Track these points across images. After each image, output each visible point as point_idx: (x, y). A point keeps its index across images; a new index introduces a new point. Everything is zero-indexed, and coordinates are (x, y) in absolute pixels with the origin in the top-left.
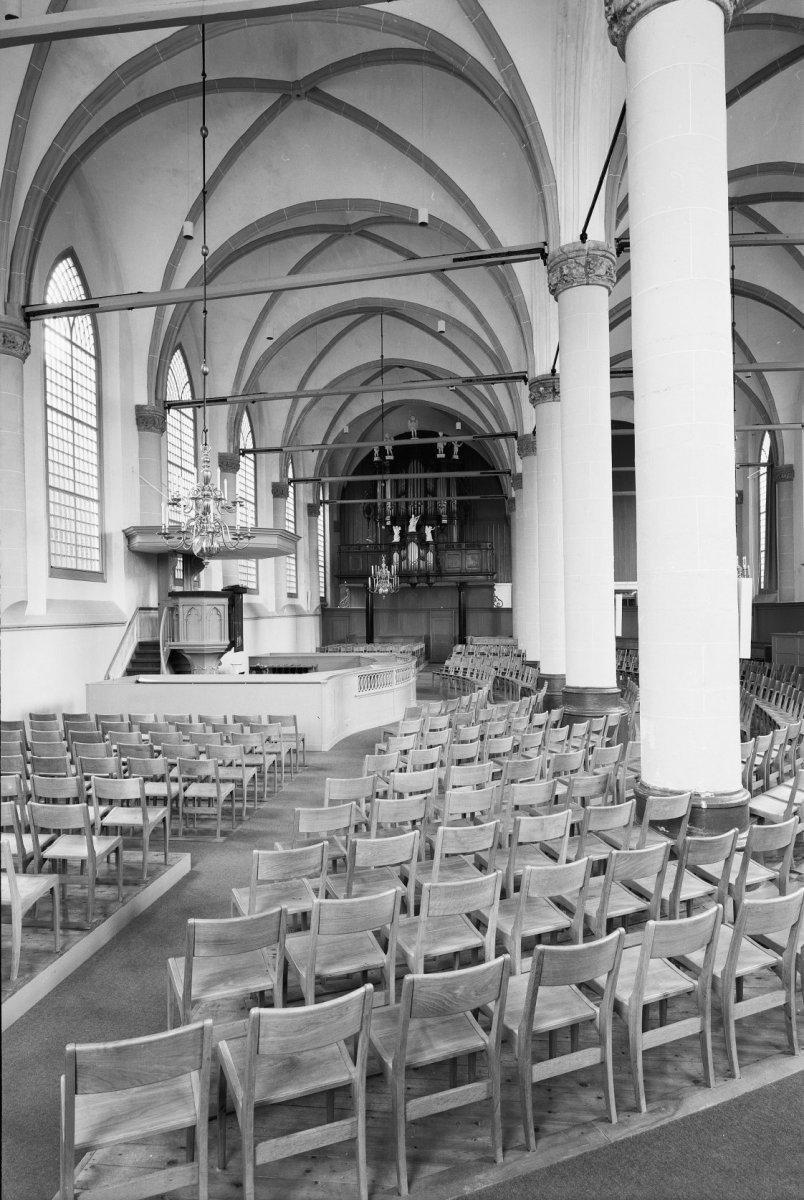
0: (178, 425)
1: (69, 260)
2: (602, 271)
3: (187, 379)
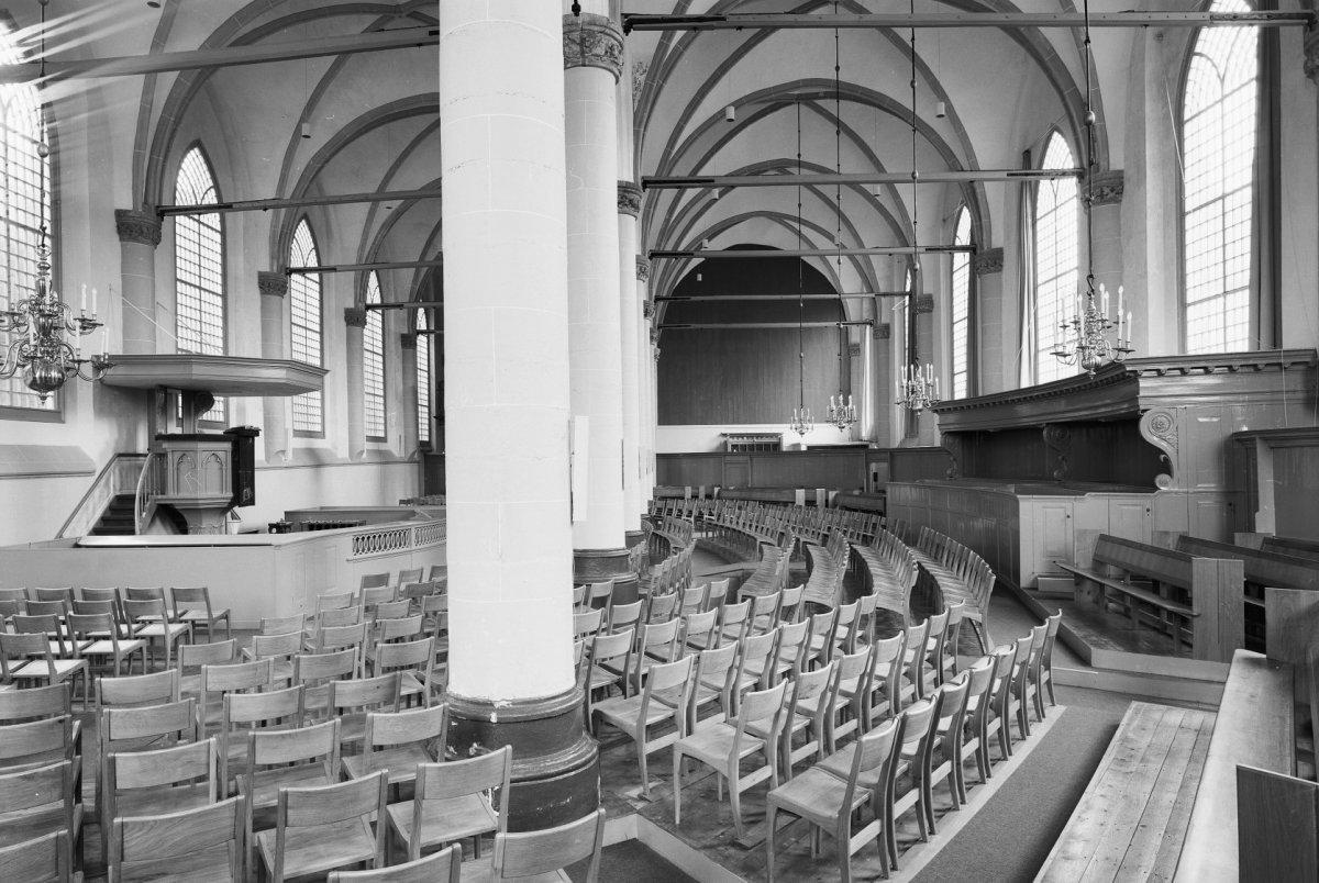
0: (302, 289)
1: (196, 150)
2: (600, 50)
3: (313, 246)
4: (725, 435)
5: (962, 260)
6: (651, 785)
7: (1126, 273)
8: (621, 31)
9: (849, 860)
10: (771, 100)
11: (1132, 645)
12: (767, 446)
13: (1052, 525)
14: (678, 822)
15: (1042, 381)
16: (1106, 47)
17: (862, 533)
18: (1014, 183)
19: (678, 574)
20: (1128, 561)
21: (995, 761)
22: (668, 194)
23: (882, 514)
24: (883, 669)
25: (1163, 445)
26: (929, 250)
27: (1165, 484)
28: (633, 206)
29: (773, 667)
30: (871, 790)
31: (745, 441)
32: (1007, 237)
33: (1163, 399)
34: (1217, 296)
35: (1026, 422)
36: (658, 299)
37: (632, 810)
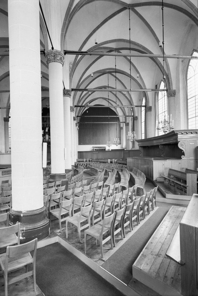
2: (58, 58)
4: (93, 147)
5: (143, 109)
6: (62, 229)
7: (176, 112)
8: (64, 54)
9: (102, 246)
10: (102, 73)
11: (175, 193)
12: (103, 149)
13: (160, 167)
14: (67, 238)
15: (160, 135)
16: (171, 63)
17: (121, 169)
18: (153, 92)
19: (79, 179)
20: (175, 174)
21: (141, 220)
22: (79, 93)
23: (126, 164)
24: (117, 200)
25: (183, 149)
26: (136, 106)
27: (183, 157)
28: (69, 95)
29: (93, 201)
30: (109, 229)
31: (98, 149)
32: (152, 104)
33: (183, 139)
34: (194, 117)
35: (155, 144)
36: (77, 116)
37: (57, 235)
